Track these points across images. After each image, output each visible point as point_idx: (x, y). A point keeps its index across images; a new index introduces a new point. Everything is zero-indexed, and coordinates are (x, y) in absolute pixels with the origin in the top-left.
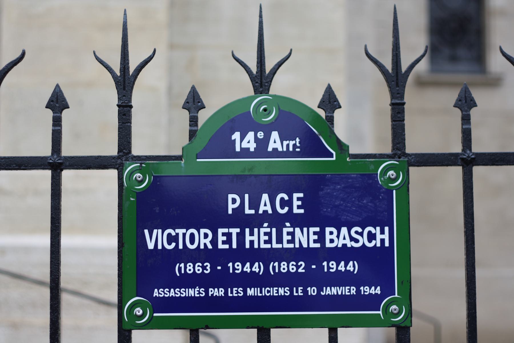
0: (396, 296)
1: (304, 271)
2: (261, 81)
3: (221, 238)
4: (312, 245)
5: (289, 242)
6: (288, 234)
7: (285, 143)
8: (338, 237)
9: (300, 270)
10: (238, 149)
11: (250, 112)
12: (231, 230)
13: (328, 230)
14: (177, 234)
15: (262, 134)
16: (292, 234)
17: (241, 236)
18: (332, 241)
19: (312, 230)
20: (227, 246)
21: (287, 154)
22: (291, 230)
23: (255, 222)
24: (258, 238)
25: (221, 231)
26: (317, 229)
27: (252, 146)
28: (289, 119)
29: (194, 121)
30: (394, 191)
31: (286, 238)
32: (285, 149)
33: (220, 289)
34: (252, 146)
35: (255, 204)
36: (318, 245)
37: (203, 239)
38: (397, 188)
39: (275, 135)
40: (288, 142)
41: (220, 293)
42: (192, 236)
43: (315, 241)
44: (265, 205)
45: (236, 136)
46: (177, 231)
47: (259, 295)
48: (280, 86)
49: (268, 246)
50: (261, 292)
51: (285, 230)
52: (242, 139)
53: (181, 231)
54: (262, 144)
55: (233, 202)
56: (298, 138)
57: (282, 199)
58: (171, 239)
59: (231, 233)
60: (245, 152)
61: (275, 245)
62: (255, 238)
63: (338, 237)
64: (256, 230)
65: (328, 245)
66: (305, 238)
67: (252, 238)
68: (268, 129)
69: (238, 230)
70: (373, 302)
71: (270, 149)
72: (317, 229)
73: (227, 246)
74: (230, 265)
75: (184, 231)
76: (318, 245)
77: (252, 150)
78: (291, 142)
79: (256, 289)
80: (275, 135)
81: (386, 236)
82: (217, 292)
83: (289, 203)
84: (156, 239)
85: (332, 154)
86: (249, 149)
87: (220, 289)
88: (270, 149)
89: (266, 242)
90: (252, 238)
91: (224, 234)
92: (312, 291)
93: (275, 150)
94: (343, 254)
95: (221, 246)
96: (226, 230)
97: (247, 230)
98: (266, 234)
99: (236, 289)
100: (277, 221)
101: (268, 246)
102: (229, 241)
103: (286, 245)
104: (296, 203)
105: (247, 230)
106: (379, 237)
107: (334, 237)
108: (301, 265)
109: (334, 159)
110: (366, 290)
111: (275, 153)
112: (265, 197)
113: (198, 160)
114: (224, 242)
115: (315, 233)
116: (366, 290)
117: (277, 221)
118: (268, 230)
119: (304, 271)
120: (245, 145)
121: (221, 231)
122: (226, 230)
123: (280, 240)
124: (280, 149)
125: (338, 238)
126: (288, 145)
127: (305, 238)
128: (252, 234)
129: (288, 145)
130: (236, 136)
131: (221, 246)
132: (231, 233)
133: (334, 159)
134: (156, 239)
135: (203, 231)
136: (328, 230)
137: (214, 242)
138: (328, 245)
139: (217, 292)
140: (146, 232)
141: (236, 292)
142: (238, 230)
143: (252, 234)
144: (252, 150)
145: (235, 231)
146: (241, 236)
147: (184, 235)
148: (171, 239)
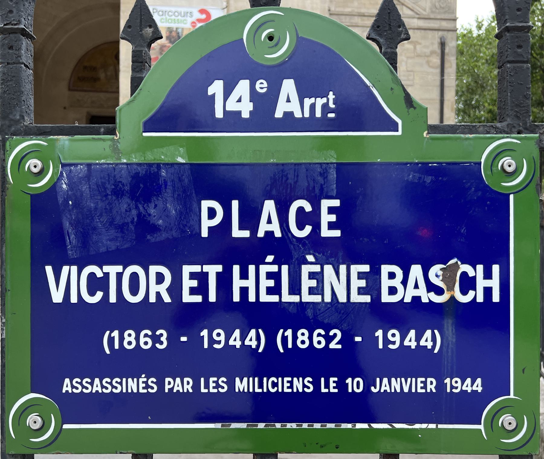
0: (512, 396)
1: (339, 347)
3: (188, 283)
4: (356, 298)
5: (311, 291)
6: (312, 276)
7: (308, 102)
8: (405, 282)
10: (219, 114)
11: (242, 39)
12: (206, 268)
13: (386, 269)
14: (107, 275)
15: (265, 85)
17: (224, 281)
18: (393, 291)
19: (356, 269)
20: (198, 299)
21: (309, 124)
22: (317, 268)
23: (251, 253)
24: (254, 284)
25: (187, 269)
26: (366, 268)
27: (246, 109)
30: (512, 197)
31: (306, 283)
33: (186, 380)
34: (246, 109)
35: (250, 219)
36: (367, 299)
37: (153, 284)
38: (519, 190)
39: (289, 87)
40: (312, 100)
41: (186, 386)
42: (134, 277)
43: (361, 291)
44: (269, 223)
45: (216, 88)
46: (106, 269)
49: (274, 298)
51: (306, 269)
52: (227, 94)
53: (113, 270)
54: (264, 103)
55: (209, 215)
56: (331, 93)
59: (207, 274)
60: (233, 121)
61: (287, 298)
62: (250, 283)
63: (405, 282)
64: (252, 268)
65: (386, 298)
66: (343, 283)
68: (275, 75)
69: (219, 268)
71: (279, 114)
72: (366, 268)
73: (198, 299)
74: (205, 333)
75: (119, 268)
76: (367, 299)
77: (246, 115)
78: (318, 99)
80: (289, 87)
82: (181, 385)
84: (68, 284)
85: (397, 124)
86: (239, 113)
87: (186, 380)
88: (279, 114)
89: (270, 291)
90: (244, 283)
91: (193, 276)
92: (354, 385)
93: (288, 115)
96: (197, 268)
97: (236, 269)
98: (270, 276)
99: (215, 379)
100: (285, 250)
101: (274, 298)
102: (202, 289)
103: (307, 298)
104: (326, 218)
105: (236, 269)
106: (481, 283)
107: (397, 282)
109: (400, 133)
110: (457, 385)
111: (289, 122)
114: (193, 291)
115: (361, 275)
116: (457, 385)
117: (285, 250)
118: (274, 268)
119: (339, 347)
120: (232, 106)
121: (187, 269)
122: (197, 268)
123: (295, 289)
124: (298, 114)
125: (405, 284)
126: (313, 107)
127: (343, 283)
128: (244, 275)
129: (313, 107)
132: (207, 274)
133: (400, 133)
134: (68, 284)
135: (154, 269)
136: (386, 269)
137: (175, 289)
138: (386, 298)
139: (181, 385)
140: (49, 269)
141: (216, 385)
142: (219, 268)
143: (244, 275)
144: (246, 115)
145: (213, 270)
146: (224, 281)
147: (119, 276)
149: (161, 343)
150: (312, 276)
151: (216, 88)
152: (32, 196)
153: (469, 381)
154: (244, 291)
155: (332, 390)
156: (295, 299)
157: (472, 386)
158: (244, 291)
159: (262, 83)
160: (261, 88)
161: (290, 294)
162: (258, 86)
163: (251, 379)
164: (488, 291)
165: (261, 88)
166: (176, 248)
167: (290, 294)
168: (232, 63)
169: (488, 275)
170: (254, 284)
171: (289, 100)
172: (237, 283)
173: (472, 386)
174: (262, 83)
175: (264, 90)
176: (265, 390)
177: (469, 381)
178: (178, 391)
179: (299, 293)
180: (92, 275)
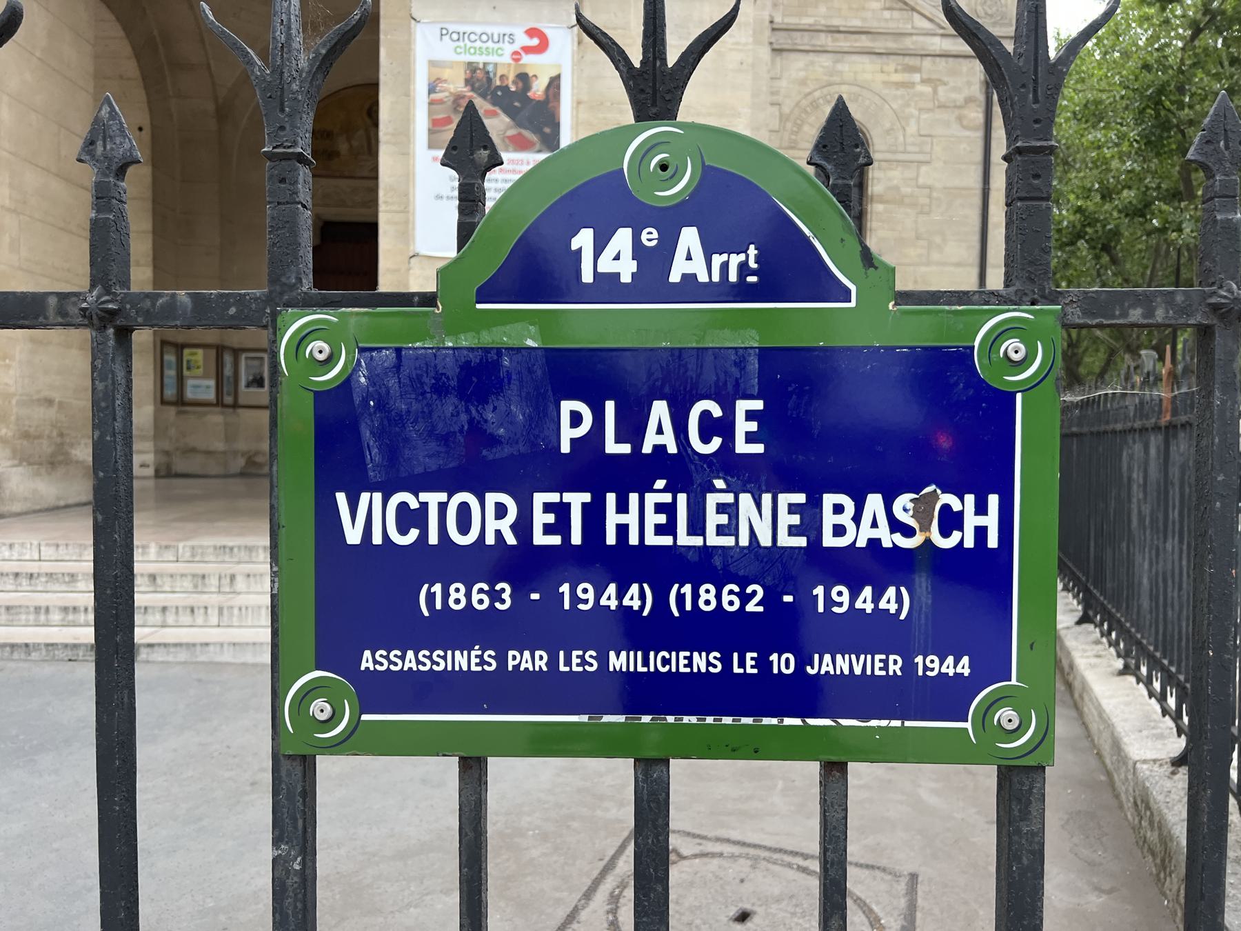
0: (1014, 681)
1: (761, 609)
2: (655, 87)
3: (541, 518)
4: (785, 540)
5: (721, 531)
6: (721, 508)
7: (717, 260)
8: (857, 519)
9: (751, 607)
10: (587, 277)
12: (568, 497)
13: (829, 500)
14: (424, 506)
15: (655, 235)
16: (730, 510)
17: (594, 515)
19: (785, 499)
20: (556, 540)
22: (729, 498)
23: (634, 475)
24: (637, 519)
25: (540, 499)
26: (800, 498)
27: (627, 269)
28: (727, 199)
29: (470, 199)
30: (1019, 396)
31: (713, 519)
32: (716, 278)
33: (538, 653)
34: (627, 269)
35: (632, 428)
36: (801, 542)
37: (491, 518)
39: (689, 238)
40: (724, 257)
41: (538, 663)
42: (464, 509)
43: (793, 530)
44: (659, 433)
46: (424, 496)
47: (641, 669)
48: (700, 101)
49: (667, 541)
50: (646, 663)
51: (712, 500)
52: (598, 252)
53: (433, 499)
54: (652, 263)
57: (705, 415)
58: (407, 517)
60: (607, 287)
61: (684, 539)
62: (631, 519)
63: (857, 519)
64: (634, 498)
65: (829, 541)
66: (767, 520)
67: (623, 519)
69: (586, 497)
70: (948, 699)
71: (675, 277)
72: (800, 498)
73: (556, 540)
74: (565, 588)
75: (443, 497)
76: (801, 542)
77: (626, 278)
79: (632, 653)
80: (689, 238)
81: (991, 521)
82: (532, 661)
83: (724, 427)
84: (368, 518)
85: (848, 291)
87: (538, 653)
88: (675, 277)
90: (623, 519)
91: (548, 508)
93: (689, 278)
94: (875, 566)
95: (540, 539)
96: (554, 497)
97: (611, 498)
98: (659, 508)
100: (682, 471)
101: (667, 541)
102: (561, 526)
103: (713, 540)
104: (743, 427)
105: (611, 498)
106: (971, 521)
107: (846, 519)
108: (754, 593)
109: (853, 304)
110: (932, 665)
111: (690, 289)
112: (660, 410)
113: (479, 306)
114: (548, 529)
115: (792, 508)
116: (932, 665)
117: (682, 471)
118: (667, 498)
119: (761, 609)
121: (540, 499)
122: (554, 497)
123: (697, 526)
124: (703, 278)
126: (725, 267)
127: (767, 520)
128: (622, 508)
129: (725, 267)
130: (584, 240)
131: (540, 539)
133: (853, 304)
134: (368, 518)
135: (492, 498)
136: (829, 500)
137: (523, 527)
138: (829, 541)
139: (532, 661)
140: (341, 498)
142: (586, 497)
143: (622, 508)
144: (626, 278)
145: (577, 500)
146: (594, 515)
147: (443, 507)
148: (407, 517)
149: (503, 601)
150: (721, 508)
151: (584, 240)
152: (316, 393)
153: (950, 660)
154: (622, 530)
155: (749, 670)
156: (697, 541)
157: (955, 667)
158: (622, 530)
159: (650, 233)
160: (650, 240)
161: (689, 534)
162: (644, 237)
163: (632, 653)
164: (981, 532)
165: (650, 240)
166: (529, 465)
167: (689, 534)
168: (606, 202)
169: (981, 509)
170: (637, 519)
171: (690, 257)
172: (613, 519)
173: (955, 667)
174: (650, 233)
175: (654, 243)
176: (652, 669)
177: (950, 660)
178: (527, 669)
179: (703, 534)
180: (403, 506)
